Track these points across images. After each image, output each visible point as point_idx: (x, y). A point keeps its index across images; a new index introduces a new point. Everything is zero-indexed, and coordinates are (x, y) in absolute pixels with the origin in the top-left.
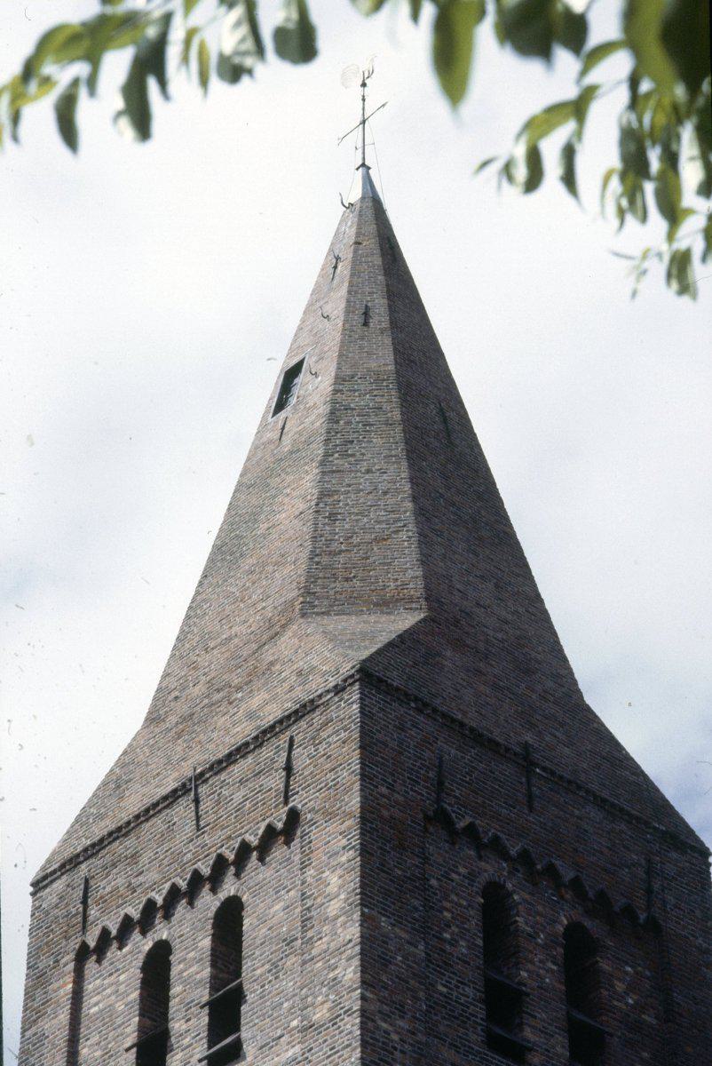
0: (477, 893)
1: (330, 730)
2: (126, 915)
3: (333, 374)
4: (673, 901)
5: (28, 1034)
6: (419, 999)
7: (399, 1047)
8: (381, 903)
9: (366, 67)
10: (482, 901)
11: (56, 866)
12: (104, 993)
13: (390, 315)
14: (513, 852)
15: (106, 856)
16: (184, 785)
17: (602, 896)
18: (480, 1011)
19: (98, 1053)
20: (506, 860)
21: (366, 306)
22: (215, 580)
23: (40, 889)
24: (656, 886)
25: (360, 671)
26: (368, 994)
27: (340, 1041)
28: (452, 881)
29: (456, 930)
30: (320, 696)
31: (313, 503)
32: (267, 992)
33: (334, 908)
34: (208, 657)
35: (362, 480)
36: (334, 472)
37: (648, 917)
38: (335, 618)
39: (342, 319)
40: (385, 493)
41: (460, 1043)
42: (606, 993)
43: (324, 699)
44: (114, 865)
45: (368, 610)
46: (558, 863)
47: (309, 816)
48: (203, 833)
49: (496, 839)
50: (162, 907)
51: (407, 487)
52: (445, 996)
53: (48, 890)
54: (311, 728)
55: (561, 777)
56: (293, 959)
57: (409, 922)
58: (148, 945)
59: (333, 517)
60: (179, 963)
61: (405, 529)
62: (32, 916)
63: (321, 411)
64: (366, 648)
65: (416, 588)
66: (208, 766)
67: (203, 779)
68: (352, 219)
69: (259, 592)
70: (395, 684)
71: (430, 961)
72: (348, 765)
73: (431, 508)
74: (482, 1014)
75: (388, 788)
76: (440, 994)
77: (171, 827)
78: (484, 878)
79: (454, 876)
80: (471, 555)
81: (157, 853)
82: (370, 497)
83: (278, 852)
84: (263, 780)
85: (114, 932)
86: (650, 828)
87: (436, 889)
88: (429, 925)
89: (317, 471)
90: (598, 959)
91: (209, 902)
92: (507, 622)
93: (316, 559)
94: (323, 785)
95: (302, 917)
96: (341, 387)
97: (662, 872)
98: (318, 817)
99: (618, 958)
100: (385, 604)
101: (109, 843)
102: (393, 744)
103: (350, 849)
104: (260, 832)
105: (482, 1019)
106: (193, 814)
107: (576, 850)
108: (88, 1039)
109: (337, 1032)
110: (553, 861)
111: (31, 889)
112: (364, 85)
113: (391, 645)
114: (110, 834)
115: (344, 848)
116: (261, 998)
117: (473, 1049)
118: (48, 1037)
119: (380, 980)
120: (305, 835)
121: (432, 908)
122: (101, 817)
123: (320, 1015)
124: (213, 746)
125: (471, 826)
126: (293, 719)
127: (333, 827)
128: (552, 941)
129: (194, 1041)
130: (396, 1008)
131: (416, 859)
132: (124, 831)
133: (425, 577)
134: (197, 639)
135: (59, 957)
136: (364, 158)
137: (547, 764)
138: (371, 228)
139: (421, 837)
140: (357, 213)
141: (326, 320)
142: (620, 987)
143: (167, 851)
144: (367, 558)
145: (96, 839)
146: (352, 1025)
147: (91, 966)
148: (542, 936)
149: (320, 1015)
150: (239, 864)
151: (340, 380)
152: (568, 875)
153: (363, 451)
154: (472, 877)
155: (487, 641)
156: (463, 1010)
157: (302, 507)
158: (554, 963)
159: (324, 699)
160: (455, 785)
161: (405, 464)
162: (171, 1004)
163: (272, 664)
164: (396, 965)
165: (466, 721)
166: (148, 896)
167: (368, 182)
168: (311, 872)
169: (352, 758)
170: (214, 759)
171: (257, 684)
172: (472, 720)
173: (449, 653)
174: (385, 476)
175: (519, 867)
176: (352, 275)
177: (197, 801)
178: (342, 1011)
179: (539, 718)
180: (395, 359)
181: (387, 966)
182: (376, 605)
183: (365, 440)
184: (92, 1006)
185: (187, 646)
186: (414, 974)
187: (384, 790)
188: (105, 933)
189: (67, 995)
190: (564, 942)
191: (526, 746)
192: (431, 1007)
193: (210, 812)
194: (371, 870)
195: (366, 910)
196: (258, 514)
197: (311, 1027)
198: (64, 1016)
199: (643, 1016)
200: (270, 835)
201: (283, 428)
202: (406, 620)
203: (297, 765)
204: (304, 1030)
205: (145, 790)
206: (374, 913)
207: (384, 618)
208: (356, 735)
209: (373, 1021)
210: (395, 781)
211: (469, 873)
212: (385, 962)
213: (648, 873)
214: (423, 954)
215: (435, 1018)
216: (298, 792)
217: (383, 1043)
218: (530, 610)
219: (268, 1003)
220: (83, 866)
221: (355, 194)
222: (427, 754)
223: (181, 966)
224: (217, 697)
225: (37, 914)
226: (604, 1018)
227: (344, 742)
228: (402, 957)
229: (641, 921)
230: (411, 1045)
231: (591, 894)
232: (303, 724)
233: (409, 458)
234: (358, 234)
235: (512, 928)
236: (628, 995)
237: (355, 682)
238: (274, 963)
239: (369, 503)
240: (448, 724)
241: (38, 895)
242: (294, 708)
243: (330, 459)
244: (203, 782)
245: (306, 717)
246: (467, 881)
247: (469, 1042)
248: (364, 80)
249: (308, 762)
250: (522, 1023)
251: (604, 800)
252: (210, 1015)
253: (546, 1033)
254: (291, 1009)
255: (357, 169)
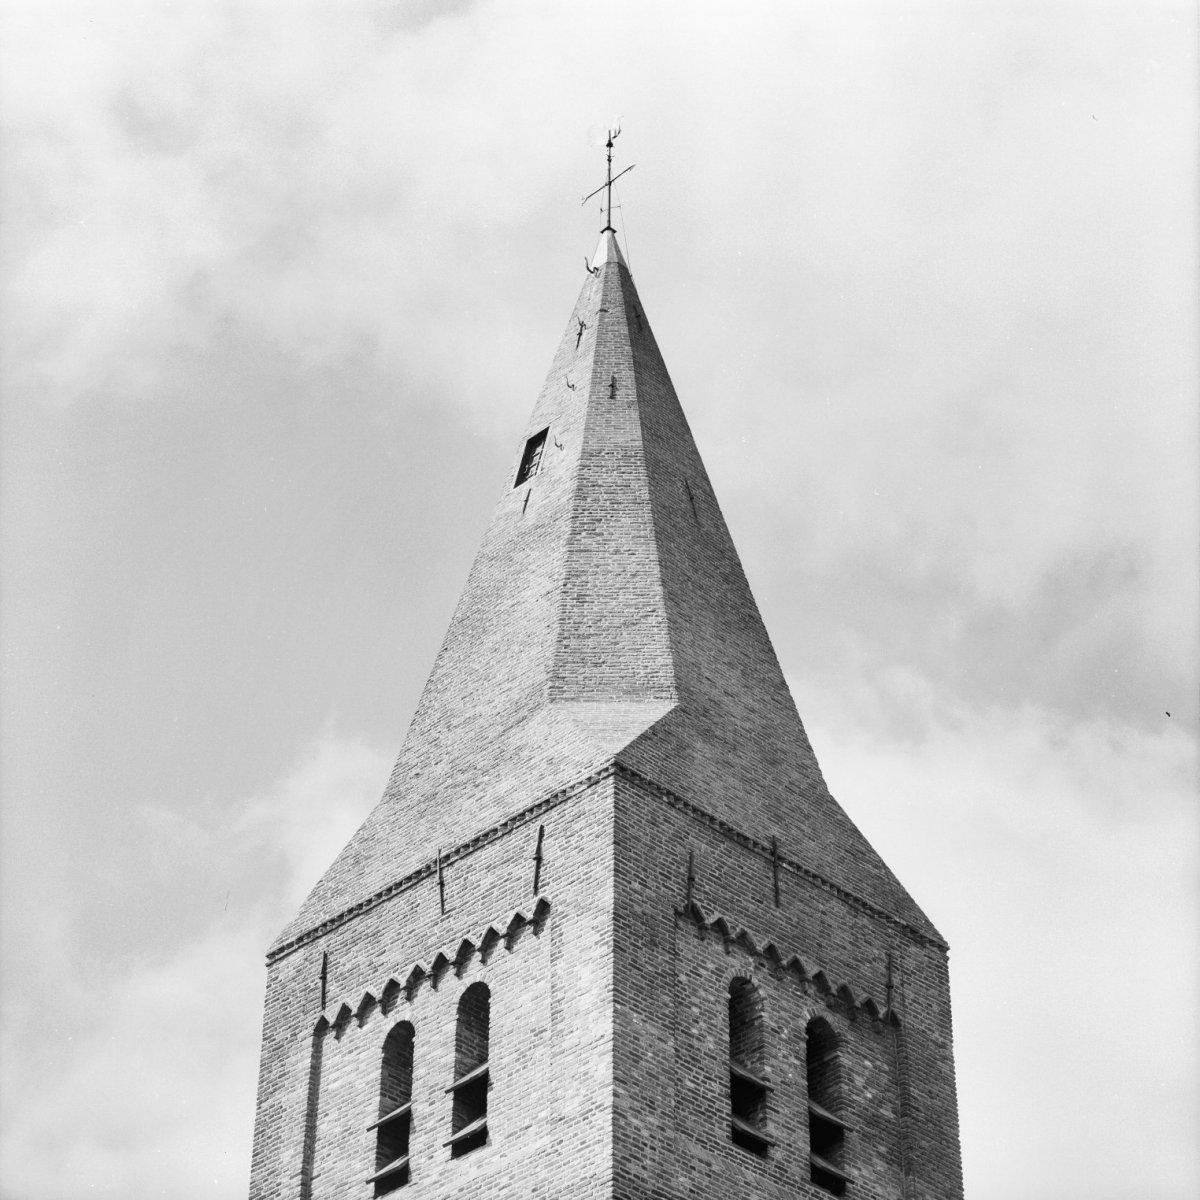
0: (724, 988)
1: (582, 823)
2: (368, 994)
3: (580, 448)
4: (912, 996)
5: (265, 1105)
6: (669, 1096)
7: (649, 1143)
8: (634, 999)
9: (614, 127)
10: (729, 996)
11: (294, 939)
12: (344, 1070)
13: (638, 388)
14: (760, 948)
15: (346, 933)
16: (428, 867)
17: (844, 990)
18: (726, 1106)
19: (339, 1130)
20: (752, 955)
21: (613, 378)
22: (457, 655)
23: (275, 962)
24: (896, 981)
25: (615, 764)
26: (620, 1091)
27: (592, 1136)
28: (700, 976)
29: (704, 1025)
30: (572, 787)
31: (561, 583)
32: (513, 1082)
33: (585, 1002)
34: (450, 735)
35: (610, 561)
36: (582, 551)
37: (888, 1011)
38: (585, 704)
39: (589, 390)
40: (634, 576)
41: (707, 1139)
42: (846, 1087)
43: (576, 791)
44: (355, 943)
45: (618, 697)
46: (802, 959)
47: (560, 908)
48: (448, 917)
49: (743, 935)
50: (404, 988)
51: (657, 570)
52: (693, 1092)
53: (284, 962)
54: (563, 819)
55: (807, 872)
56: (540, 1050)
57: (659, 1018)
58: (388, 1023)
59: (581, 599)
60: (423, 1045)
61: (655, 614)
62: (268, 987)
63: (568, 485)
64: (619, 740)
65: (666, 677)
66: (453, 850)
67: (449, 862)
68: (597, 284)
69: (505, 671)
70: (648, 778)
71: (678, 1057)
72: (602, 860)
73: (679, 592)
74: (728, 1109)
75: (640, 883)
76: (689, 1090)
77: (414, 907)
78: (730, 974)
79: (702, 972)
80: (719, 641)
81: (399, 933)
82: (619, 579)
83: (526, 940)
84: (510, 868)
85: (355, 1011)
86: (891, 922)
87: (686, 985)
88: (678, 1020)
89: (565, 549)
90: (839, 1053)
91: (453, 986)
92: (753, 711)
93: (565, 642)
94: (575, 878)
95: (552, 1009)
96: (588, 462)
97: (902, 966)
98: (570, 910)
99: (857, 1053)
100: (634, 692)
101: (349, 920)
102: (646, 840)
103: (603, 945)
104: (509, 921)
105: (727, 1114)
106: (439, 896)
107: (820, 945)
108: (327, 1115)
109: (588, 1127)
110: (798, 956)
111: (267, 961)
112: (610, 145)
113: (643, 737)
114: (350, 911)
115: (596, 943)
116: (508, 1087)
117: (718, 1144)
118: (285, 1110)
119: (632, 1077)
120: (556, 927)
121: (681, 1003)
122: (338, 892)
123: (570, 1108)
124: (459, 829)
125: (720, 923)
126: (544, 808)
127: (586, 921)
128: (795, 1036)
129: (438, 1124)
130: (647, 1104)
131: (668, 955)
132: (365, 908)
133: (675, 665)
134: (438, 715)
135: (297, 1031)
136: (609, 221)
137: (795, 859)
138: (617, 295)
139: (672, 932)
140: (602, 278)
141: (571, 390)
142: (859, 1081)
143: (410, 933)
144: (616, 644)
145: (336, 915)
146: (604, 1120)
147: (329, 1039)
148: (786, 1031)
149: (570, 1108)
150: (485, 951)
151: (587, 454)
152: (812, 970)
153: (611, 530)
154: (719, 972)
155: (735, 731)
156: (709, 1106)
157: (550, 586)
158: (796, 1057)
159: (576, 791)
160: (705, 880)
161: (653, 546)
162: (414, 1086)
163: (520, 748)
164: (647, 1061)
165: (716, 815)
166: (391, 976)
167: (614, 246)
168: (561, 964)
169: (604, 849)
170: (461, 843)
171: (504, 768)
172: (722, 815)
173: (699, 745)
174: (633, 558)
175: (765, 963)
176: (598, 344)
177: (442, 884)
178: (593, 1107)
179: (787, 811)
180: (643, 434)
181: (637, 1062)
182: (627, 692)
183: (613, 519)
184: (329, 1082)
185: (428, 721)
186: (663, 1070)
187: (636, 886)
188: (345, 1011)
189: (304, 1069)
190: (807, 1037)
191: (774, 841)
192: (678, 1102)
193: (456, 896)
194: (623, 966)
195: (619, 1007)
196: (503, 588)
197: (561, 1119)
198: (302, 1092)
199: (881, 1110)
200: (519, 921)
201: (527, 501)
202: (656, 710)
203: (546, 855)
204: (554, 1121)
205: (387, 868)
206: (627, 1009)
207: (634, 707)
208: (610, 830)
209: (624, 1117)
210: (648, 877)
211: (716, 969)
212: (636, 1058)
213: (888, 968)
214: (673, 1050)
215: (683, 1113)
216: (549, 883)
217: (634, 1139)
218: (776, 698)
219: (516, 1092)
220: (322, 941)
221: (600, 258)
222: (679, 849)
223: (425, 1048)
224: (461, 778)
225: (273, 986)
226: (843, 1112)
227: (597, 837)
228: (653, 1053)
229: (881, 1016)
230: (660, 1141)
231: (834, 990)
232: (554, 813)
233: (658, 539)
234: (604, 301)
235: (756, 1023)
236: (867, 1089)
237: (608, 776)
238: (522, 1053)
239: (617, 586)
240: (700, 819)
241: (274, 966)
242: (546, 797)
243: (578, 537)
244: (448, 865)
245: (558, 807)
246: (714, 977)
247: (715, 1137)
248: (610, 141)
249: (560, 853)
250: (765, 1118)
251: (847, 895)
252: (455, 1099)
253: (788, 1128)
254: (539, 1099)
255: (602, 232)
